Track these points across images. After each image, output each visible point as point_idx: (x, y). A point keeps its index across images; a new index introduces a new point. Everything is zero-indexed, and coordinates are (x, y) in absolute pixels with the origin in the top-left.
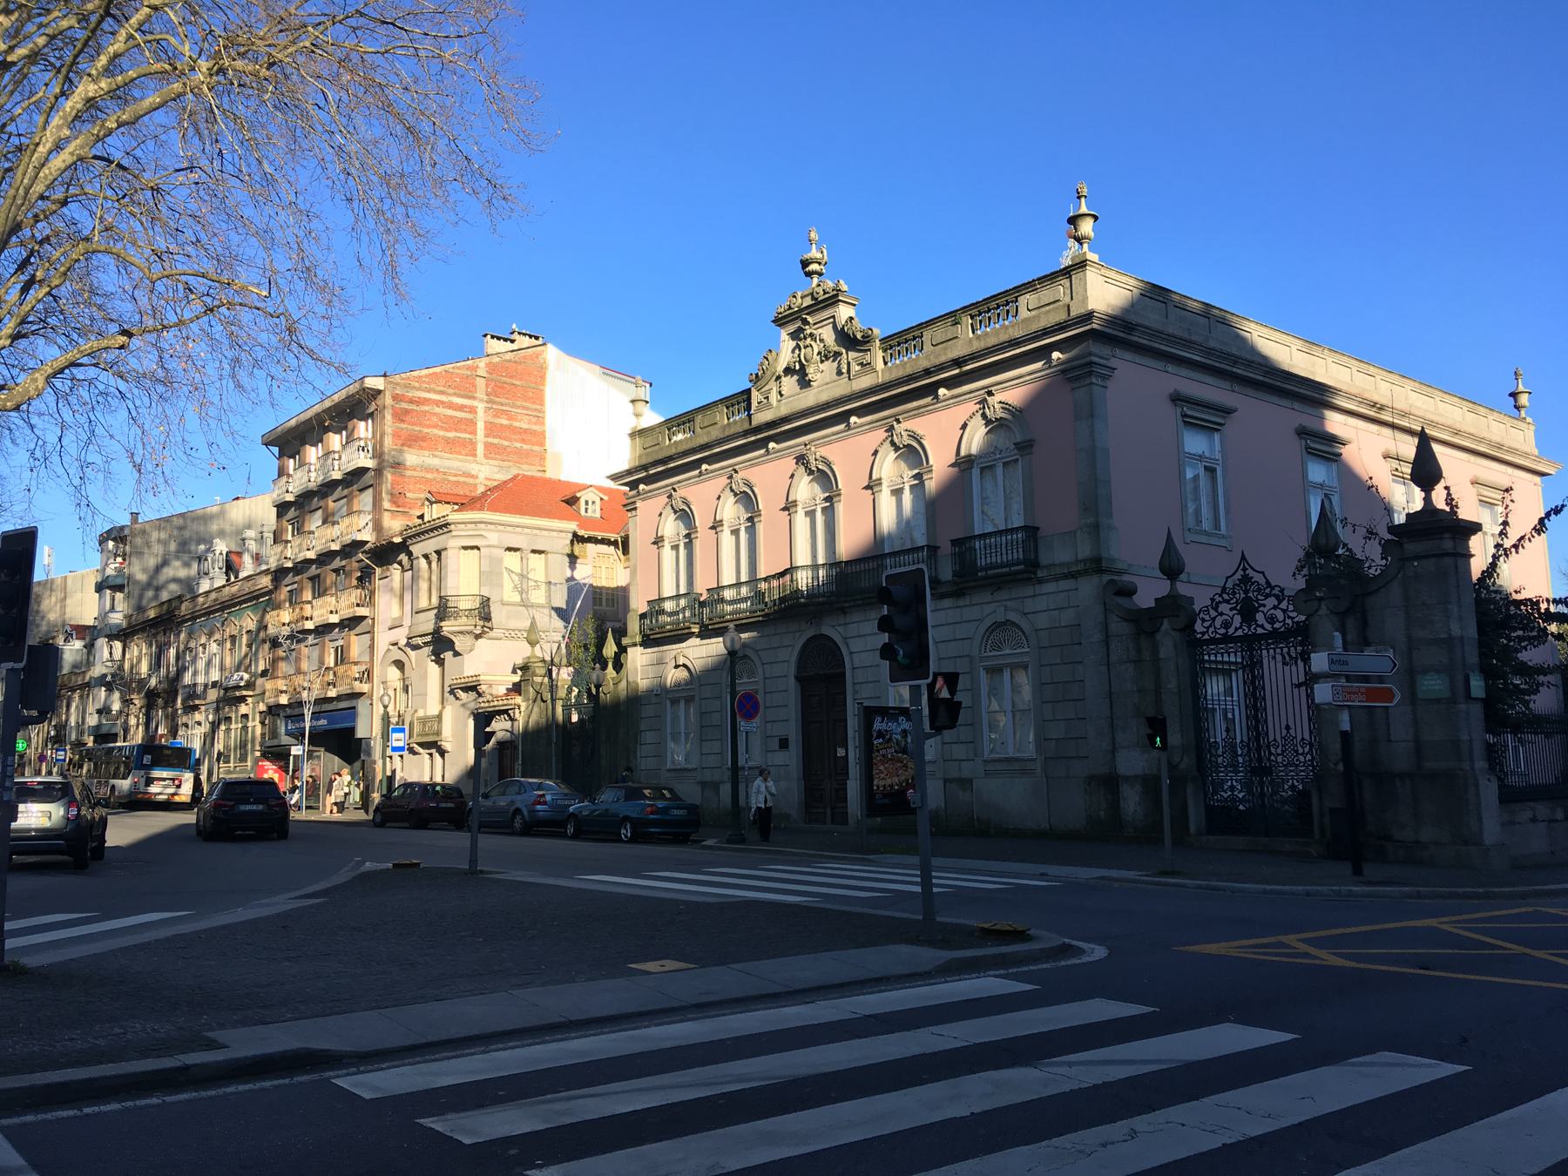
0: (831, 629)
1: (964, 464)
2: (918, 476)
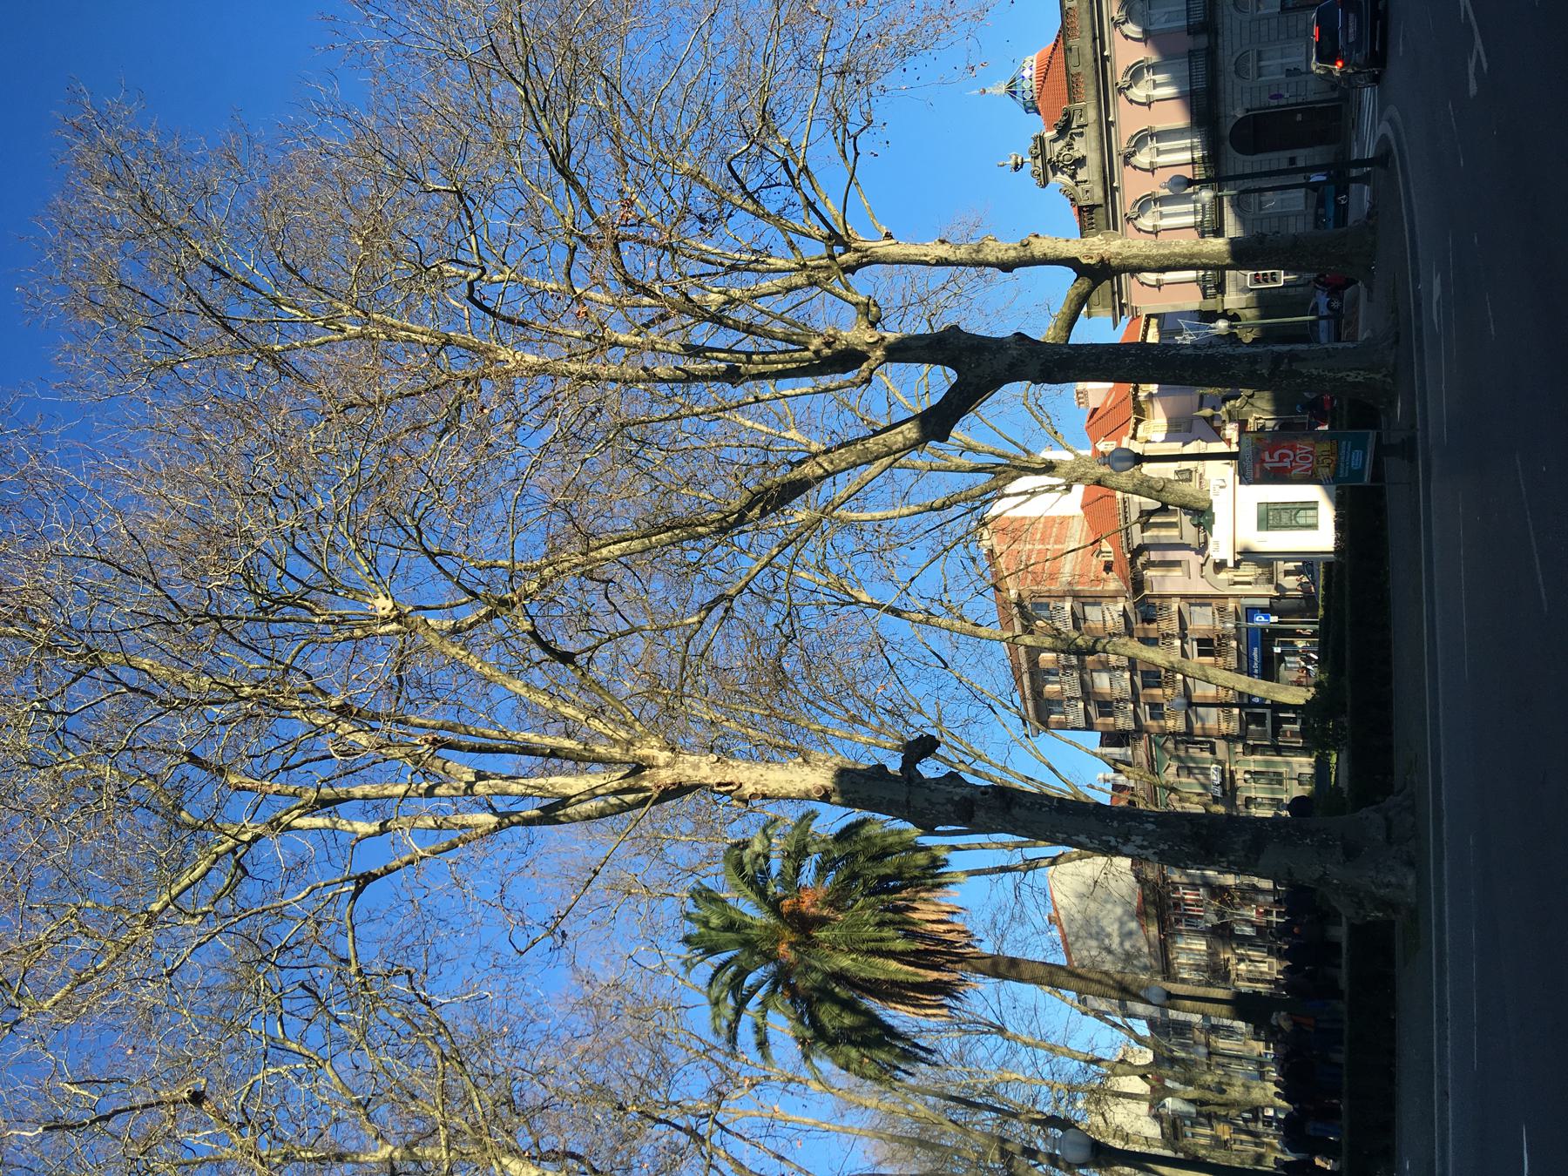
0: (1227, 128)
1: (1147, 36)
2: (1148, 68)
